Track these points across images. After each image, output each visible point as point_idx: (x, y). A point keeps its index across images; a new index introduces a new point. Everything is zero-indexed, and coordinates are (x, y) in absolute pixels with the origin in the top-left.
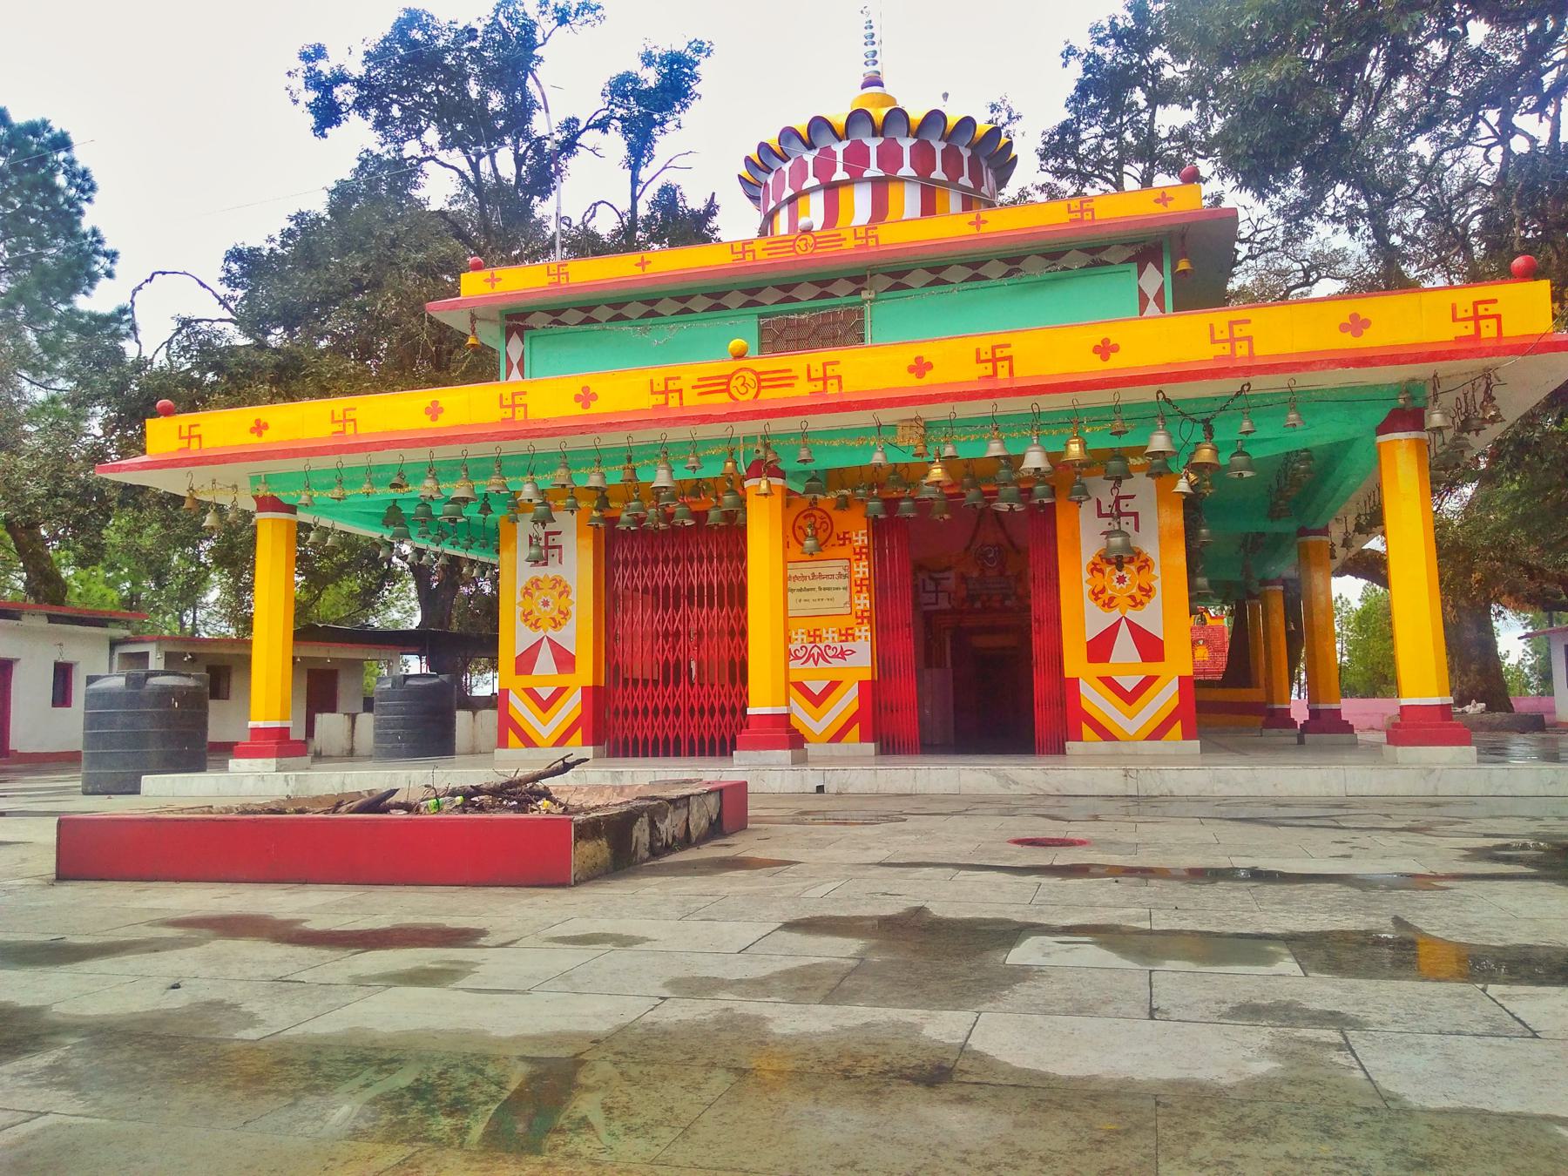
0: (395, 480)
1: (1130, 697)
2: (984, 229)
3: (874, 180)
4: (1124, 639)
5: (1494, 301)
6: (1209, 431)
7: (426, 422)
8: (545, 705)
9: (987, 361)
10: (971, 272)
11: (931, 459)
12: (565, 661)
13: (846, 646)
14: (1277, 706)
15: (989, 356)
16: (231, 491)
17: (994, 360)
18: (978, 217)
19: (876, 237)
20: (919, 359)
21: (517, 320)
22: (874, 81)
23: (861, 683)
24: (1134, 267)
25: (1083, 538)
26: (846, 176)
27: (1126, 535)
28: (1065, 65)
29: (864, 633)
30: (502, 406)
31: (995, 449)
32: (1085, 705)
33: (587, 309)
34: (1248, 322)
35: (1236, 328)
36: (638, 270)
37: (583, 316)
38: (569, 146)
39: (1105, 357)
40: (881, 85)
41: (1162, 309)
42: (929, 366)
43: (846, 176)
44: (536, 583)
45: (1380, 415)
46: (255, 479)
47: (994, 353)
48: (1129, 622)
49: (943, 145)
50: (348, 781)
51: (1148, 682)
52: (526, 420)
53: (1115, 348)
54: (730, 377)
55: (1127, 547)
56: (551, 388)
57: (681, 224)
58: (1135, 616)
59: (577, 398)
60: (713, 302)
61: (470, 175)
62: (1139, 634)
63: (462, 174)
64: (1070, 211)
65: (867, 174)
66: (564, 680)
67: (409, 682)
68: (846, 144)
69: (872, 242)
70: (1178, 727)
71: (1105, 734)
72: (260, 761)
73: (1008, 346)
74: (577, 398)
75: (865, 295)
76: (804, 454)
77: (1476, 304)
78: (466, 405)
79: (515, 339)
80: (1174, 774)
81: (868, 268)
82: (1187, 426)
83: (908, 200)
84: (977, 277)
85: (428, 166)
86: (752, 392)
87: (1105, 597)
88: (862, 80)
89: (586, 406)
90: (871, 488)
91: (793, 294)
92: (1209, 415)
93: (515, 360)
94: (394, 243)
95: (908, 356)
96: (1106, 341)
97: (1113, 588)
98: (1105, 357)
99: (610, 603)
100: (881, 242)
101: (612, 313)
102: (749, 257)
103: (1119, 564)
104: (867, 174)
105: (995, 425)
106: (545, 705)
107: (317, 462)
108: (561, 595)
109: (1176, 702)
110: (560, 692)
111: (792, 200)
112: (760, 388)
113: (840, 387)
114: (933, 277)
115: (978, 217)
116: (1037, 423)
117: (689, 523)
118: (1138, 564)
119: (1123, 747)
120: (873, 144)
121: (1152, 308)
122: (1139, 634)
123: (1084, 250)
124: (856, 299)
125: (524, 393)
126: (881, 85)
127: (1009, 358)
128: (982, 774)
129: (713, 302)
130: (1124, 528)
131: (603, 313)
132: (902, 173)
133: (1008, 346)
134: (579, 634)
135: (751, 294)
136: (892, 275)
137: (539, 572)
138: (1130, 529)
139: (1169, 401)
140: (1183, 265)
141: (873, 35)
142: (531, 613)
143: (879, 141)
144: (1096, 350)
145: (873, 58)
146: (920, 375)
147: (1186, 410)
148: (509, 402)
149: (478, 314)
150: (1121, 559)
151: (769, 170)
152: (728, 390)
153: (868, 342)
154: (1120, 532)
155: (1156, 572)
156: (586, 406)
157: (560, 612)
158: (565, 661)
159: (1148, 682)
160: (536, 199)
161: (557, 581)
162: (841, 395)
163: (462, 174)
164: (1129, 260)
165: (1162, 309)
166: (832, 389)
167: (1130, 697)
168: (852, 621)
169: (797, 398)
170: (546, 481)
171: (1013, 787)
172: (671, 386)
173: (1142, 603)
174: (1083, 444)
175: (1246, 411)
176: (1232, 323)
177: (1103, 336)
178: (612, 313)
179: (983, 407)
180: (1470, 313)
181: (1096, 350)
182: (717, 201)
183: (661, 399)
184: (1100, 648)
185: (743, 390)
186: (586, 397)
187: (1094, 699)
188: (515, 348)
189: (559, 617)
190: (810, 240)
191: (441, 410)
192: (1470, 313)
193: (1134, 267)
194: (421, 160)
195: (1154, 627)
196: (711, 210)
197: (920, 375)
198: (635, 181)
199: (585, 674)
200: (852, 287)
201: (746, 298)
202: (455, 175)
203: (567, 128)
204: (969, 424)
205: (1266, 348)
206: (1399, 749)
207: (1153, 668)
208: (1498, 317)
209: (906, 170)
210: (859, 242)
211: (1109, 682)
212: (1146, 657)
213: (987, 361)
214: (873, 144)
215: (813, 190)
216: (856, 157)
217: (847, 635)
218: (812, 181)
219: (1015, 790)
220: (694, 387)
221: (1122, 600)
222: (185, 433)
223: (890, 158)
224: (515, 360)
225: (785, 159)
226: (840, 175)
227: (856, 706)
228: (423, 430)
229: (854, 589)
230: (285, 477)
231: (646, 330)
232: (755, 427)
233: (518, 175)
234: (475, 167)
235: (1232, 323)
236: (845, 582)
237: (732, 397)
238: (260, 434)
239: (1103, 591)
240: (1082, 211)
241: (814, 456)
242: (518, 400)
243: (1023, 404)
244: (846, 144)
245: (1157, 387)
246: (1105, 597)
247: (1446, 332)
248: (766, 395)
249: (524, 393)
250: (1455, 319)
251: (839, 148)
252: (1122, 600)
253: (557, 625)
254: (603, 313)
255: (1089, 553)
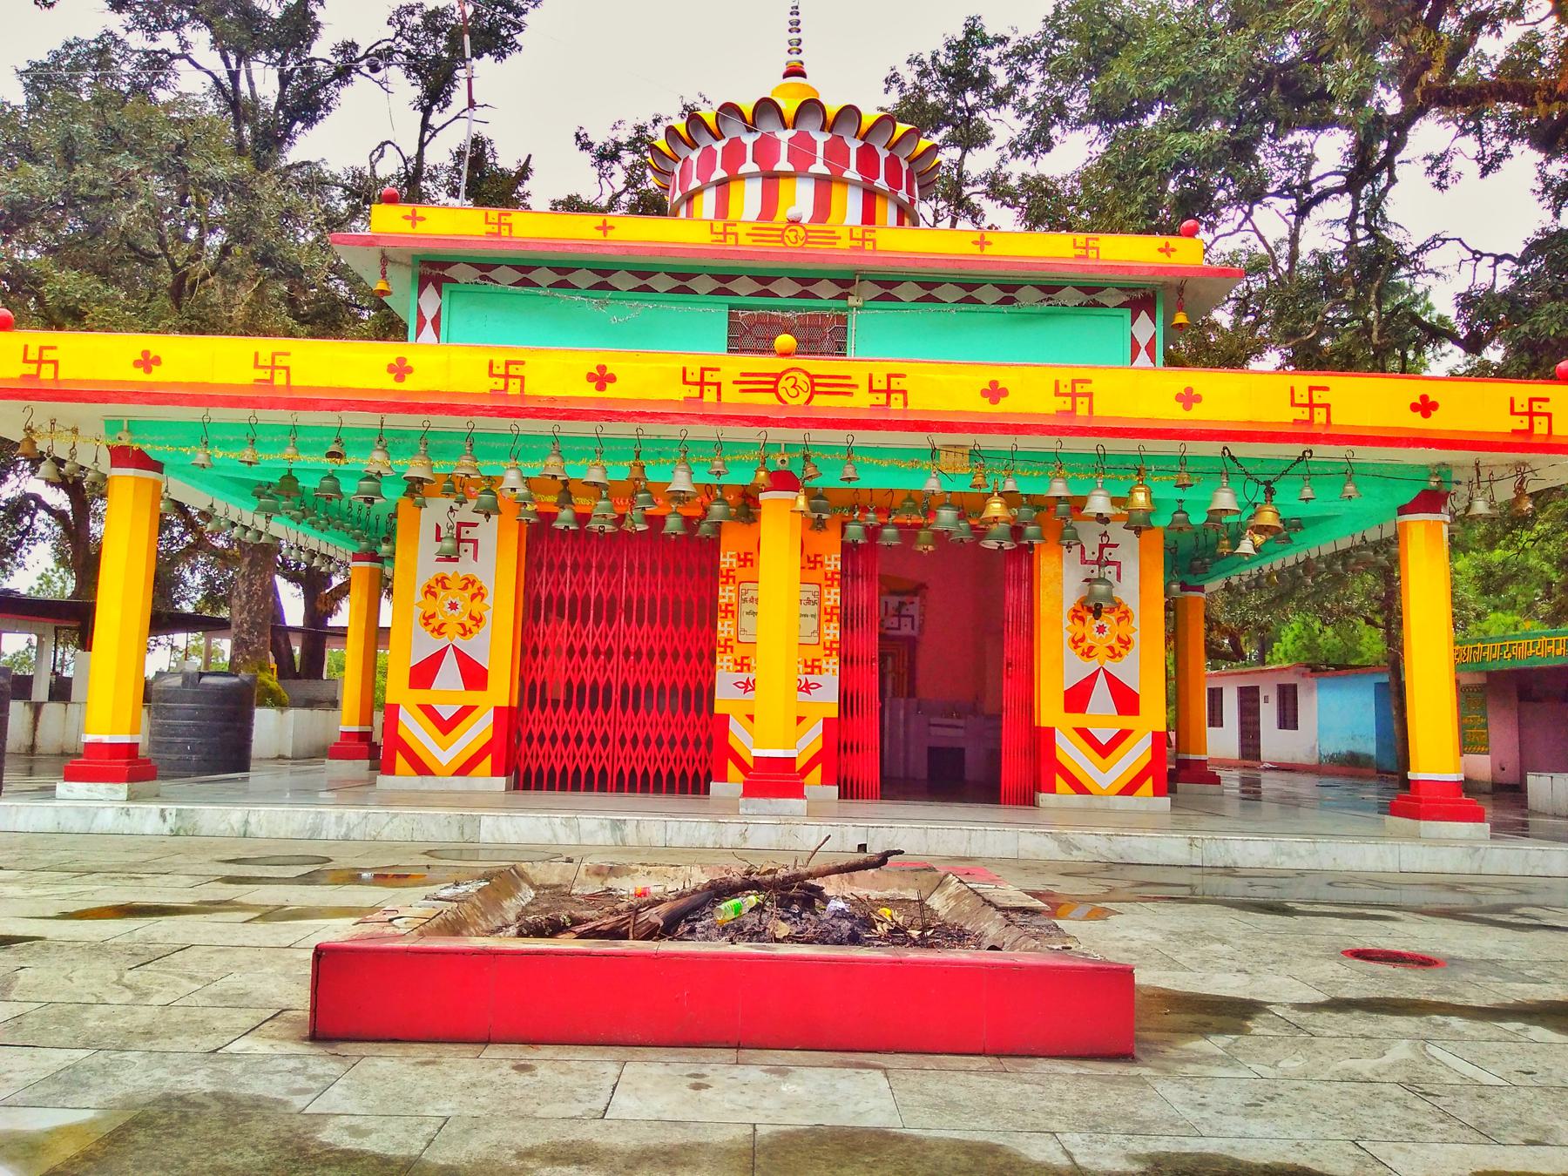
0: (333, 448)
1: (1104, 750)
2: (988, 250)
3: (819, 178)
4: (1101, 689)
5: (1546, 400)
6: (1270, 492)
7: (388, 382)
8: (446, 727)
9: (1066, 395)
10: (963, 294)
11: (989, 490)
12: (474, 676)
13: (811, 679)
14: (1191, 757)
15: (1069, 390)
16: (85, 439)
17: (1074, 395)
18: (414, 212)
19: (874, 241)
20: (994, 384)
21: (434, 270)
22: (795, 72)
23: (826, 720)
24: (1127, 313)
25: (1059, 582)
26: (790, 168)
27: (1108, 583)
28: (887, 91)
29: (832, 665)
30: (491, 375)
31: (1059, 489)
32: (1059, 756)
33: (525, 268)
34: (1326, 389)
35: (1315, 393)
36: (976, 250)
37: (518, 276)
38: (343, 74)
39: (1187, 407)
40: (803, 75)
41: (1153, 361)
42: (1004, 392)
43: (790, 168)
44: (442, 581)
45: (1408, 494)
46: (112, 424)
47: (1073, 388)
48: (1107, 674)
49: (887, 153)
50: (253, 819)
51: (1123, 735)
52: (522, 396)
53: (1198, 399)
54: (779, 376)
55: (1110, 597)
56: (450, 358)
57: (490, 184)
58: (1114, 668)
59: (591, 377)
60: (678, 283)
61: (226, 81)
62: (1116, 687)
63: (217, 82)
64: (1075, 247)
65: (813, 169)
66: (473, 697)
67: (205, 680)
68: (791, 133)
69: (1092, 254)
70: (1149, 783)
71: (1079, 788)
72: (102, 786)
73: (1088, 382)
74: (591, 377)
75: (852, 301)
76: (850, 473)
77: (1531, 400)
78: (351, 364)
79: (430, 290)
80: (1238, 845)
81: (856, 273)
82: (1252, 486)
83: (849, 205)
84: (929, 299)
85: (181, 65)
86: (804, 397)
87: (1084, 645)
88: (784, 69)
89: (601, 387)
90: (852, 511)
91: (771, 288)
92: (1271, 478)
93: (429, 315)
94: (180, 150)
95: (983, 379)
96: (1189, 390)
97: (1093, 637)
98: (1187, 407)
99: (535, 609)
100: (879, 246)
101: (556, 278)
102: (731, 240)
103: (1097, 612)
104: (813, 169)
105: (1058, 464)
106: (446, 727)
107: (219, 414)
108: (473, 597)
109: (1148, 758)
110: (466, 711)
111: (722, 184)
112: (813, 393)
113: (906, 404)
114: (925, 293)
115: (414, 212)
116: (1101, 465)
117: (641, 527)
118: (1118, 614)
119: (1095, 801)
120: (749, 140)
121: (1143, 356)
122: (1116, 687)
123: (797, 280)
124: (842, 304)
125: (522, 363)
126: (803, 75)
127: (1090, 395)
128: (1043, 839)
129: (678, 283)
130: (1108, 577)
131: (544, 277)
132: (847, 174)
133: (1088, 382)
134: (496, 647)
135: (724, 281)
136: (557, 270)
137: (448, 569)
138: (1112, 578)
139: (1233, 458)
140: (1181, 318)
141: (798, 22)
142: (433, 616)
143: (827, 137)
144: (1179, 397)
145: (796, 47)
146: (995, 401)
147: (1251, 470)
148: (502, 371)
149: (389, 252)
150: (1092, 608)
151: (693, 145)
152: (775, 391)
153: (850, 353)
154: (1102, 580)
155: (1135, 623)
156: (601, 387)
157: (472, 617)
158: (474, 676)
159: (1123, 735)
160: (299, 125)
161: (469, 582)
162: (905, 411)
163: (217, 82)
164: (1123, 305)
165: (1153, 361)
166: (897, 403)
167: (1104, 750)
168: (819, 652)
169: (856, 409)
170: (534, 469)
171: (1075, 852)
172: (708, 377)
173: (1120, 655)
174: (1149, 493)
175: (1308, 477)
176: (1311, 389)
177: (1187, 385)
178: (556, 278)
179: (1048, 443)
180: (1526, 409)
181: (1179, 397)
182: (532, 165)
183: (695, 391)
184: (1077, 699)
185: (793, 392)
186: (602, 378)
187: (1070, 751)
188: (430, 302)
189: (469, 624)
190: (802, 233)
191: (410, 370)
192: (1526, 409)
193: (1127, 313)
194: (173, 57)
195: (1131, 680)
196: (524, 172)
197: (995, 401)
198: (425, 126)
199: (501, 690)
200: (838, 291)
201: (717, 285)
202: (209, 81)
203: (344, 52)
204: (1033, 458)
205: (1344, 418)
206: (1422, 823)
207: (1127, 722)
208: (1549, 415)
209: (852, 173)
210: (855, 243)
211: (1084, 734)
212: (1121, 711)
213: (1066, 395)
214: (821, 139)
215: (750, 176)
216: (802, 152)
217: (813, 667)
218: (749, 166)
219: (1077, 856)
220: (736, 382)
221: (1101, 650)
222: (33, 354)
223: (766, 150)
224: (429, 315)
225: (718, 136)
226: (783, 165)
227: (819, 746)
228: (383, 392)
229: (825, 617)
230: (152, 428)
231: (603, 303)
232: (795, 435)
233: (281, 94)
234: (234, 76)
235: (1311, 389)
236: (814, 609)
237: (780, 398)
238: (148, 370)
239: (1083, 639)
240: (1087, 248)
241: (859, 475)
242: (512, 370)
243: (1087, 444)
244: (791, 133)
245: (1223, 444)
246: (1084, 645)
247: (1283, 414)
248: (818, 401)
249: (522, 363)
250: (1513, 413)
251: (784, 136)
252: (1101, 650)
253: (466, 632)
254: (544, 277)
255: (1071, 599)
